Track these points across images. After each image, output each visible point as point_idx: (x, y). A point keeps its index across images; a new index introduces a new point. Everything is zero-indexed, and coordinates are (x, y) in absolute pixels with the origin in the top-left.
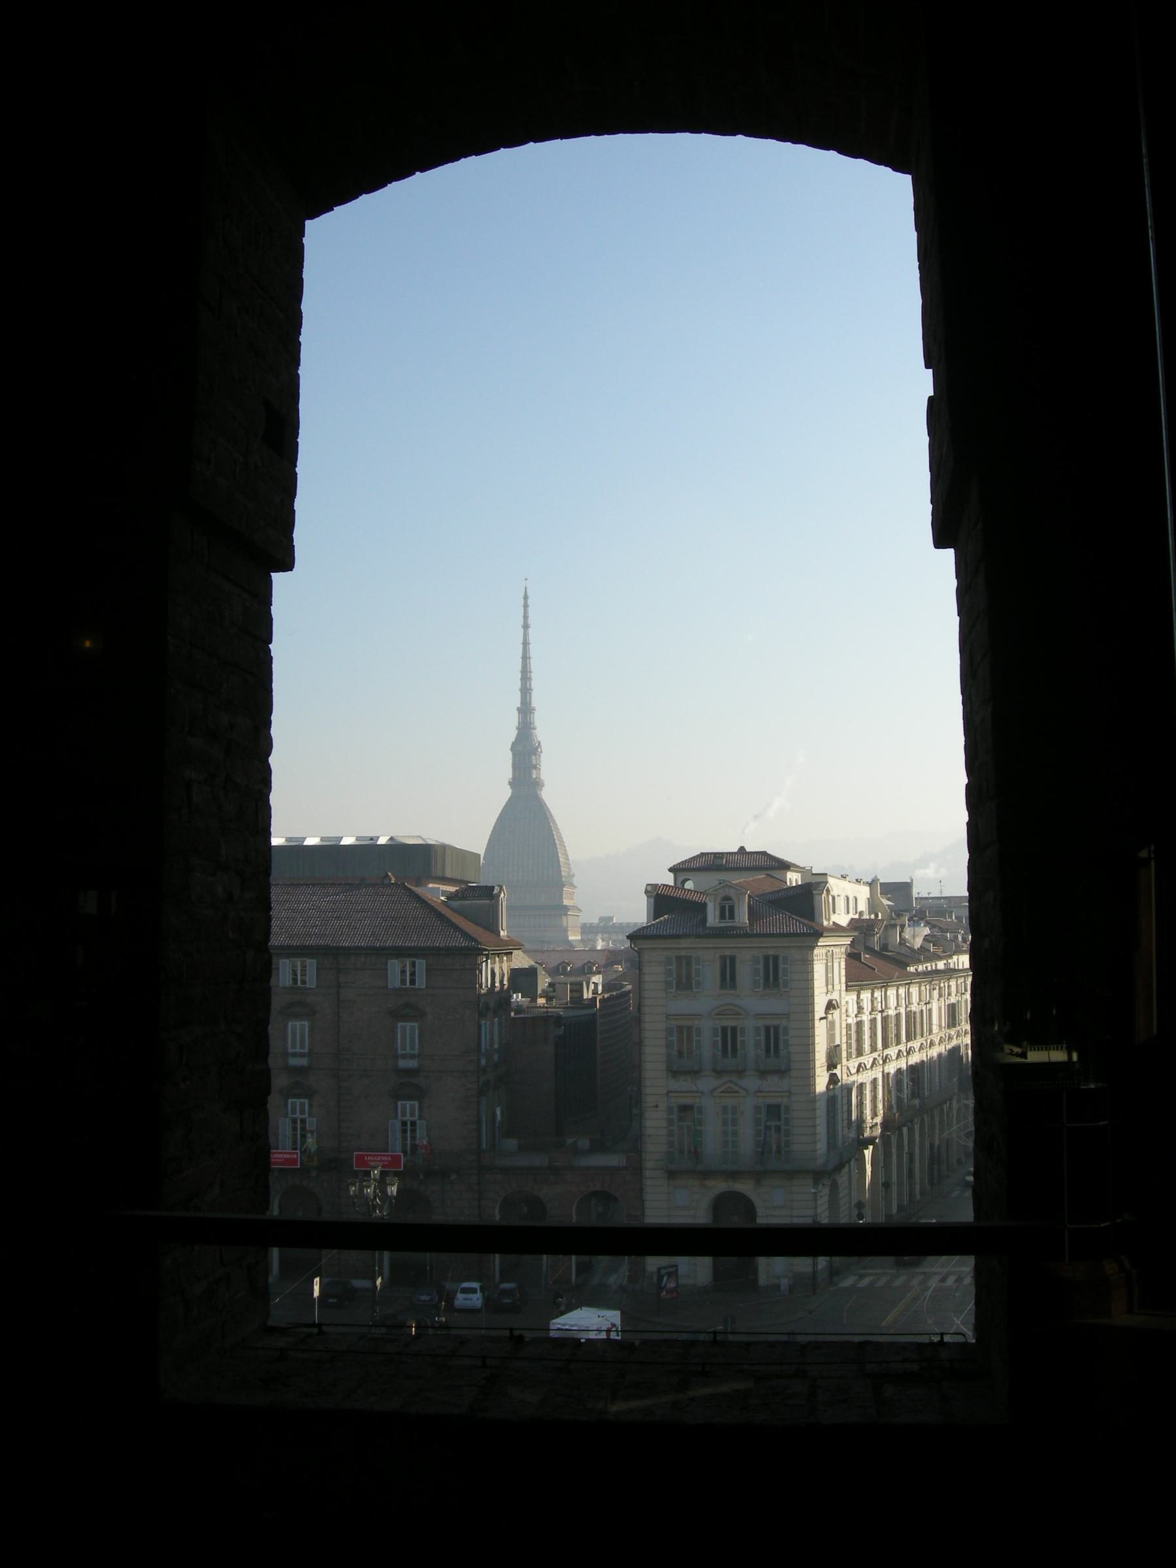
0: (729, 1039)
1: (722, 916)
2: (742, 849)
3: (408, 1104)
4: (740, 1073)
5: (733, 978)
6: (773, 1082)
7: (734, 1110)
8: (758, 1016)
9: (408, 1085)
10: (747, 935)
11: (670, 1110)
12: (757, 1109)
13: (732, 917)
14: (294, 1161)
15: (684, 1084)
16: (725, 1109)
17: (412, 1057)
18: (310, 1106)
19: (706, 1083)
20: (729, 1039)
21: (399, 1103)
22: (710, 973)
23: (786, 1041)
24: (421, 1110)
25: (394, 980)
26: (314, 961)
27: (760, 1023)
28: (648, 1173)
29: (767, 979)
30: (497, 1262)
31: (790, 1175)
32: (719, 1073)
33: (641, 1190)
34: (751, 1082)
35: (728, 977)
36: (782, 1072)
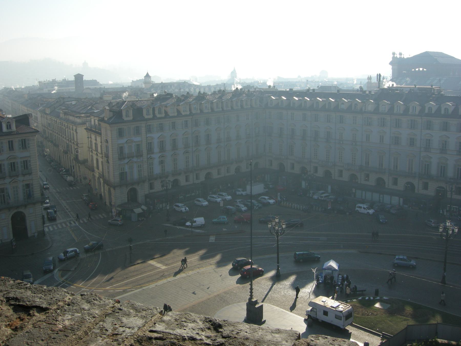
0: (13, 166)
1: (7, 128)
4: (17, 176)
5: (25, 146)
8: (21, 158)
10: (17, 134)
13: (10, 128)
19: (8, 180)
20: (13, 166)
22: (143, 130)
31: (34, 204)
32: (11, 177)
34: (21, 178)
35: (11, 147)
36: (30, 174)
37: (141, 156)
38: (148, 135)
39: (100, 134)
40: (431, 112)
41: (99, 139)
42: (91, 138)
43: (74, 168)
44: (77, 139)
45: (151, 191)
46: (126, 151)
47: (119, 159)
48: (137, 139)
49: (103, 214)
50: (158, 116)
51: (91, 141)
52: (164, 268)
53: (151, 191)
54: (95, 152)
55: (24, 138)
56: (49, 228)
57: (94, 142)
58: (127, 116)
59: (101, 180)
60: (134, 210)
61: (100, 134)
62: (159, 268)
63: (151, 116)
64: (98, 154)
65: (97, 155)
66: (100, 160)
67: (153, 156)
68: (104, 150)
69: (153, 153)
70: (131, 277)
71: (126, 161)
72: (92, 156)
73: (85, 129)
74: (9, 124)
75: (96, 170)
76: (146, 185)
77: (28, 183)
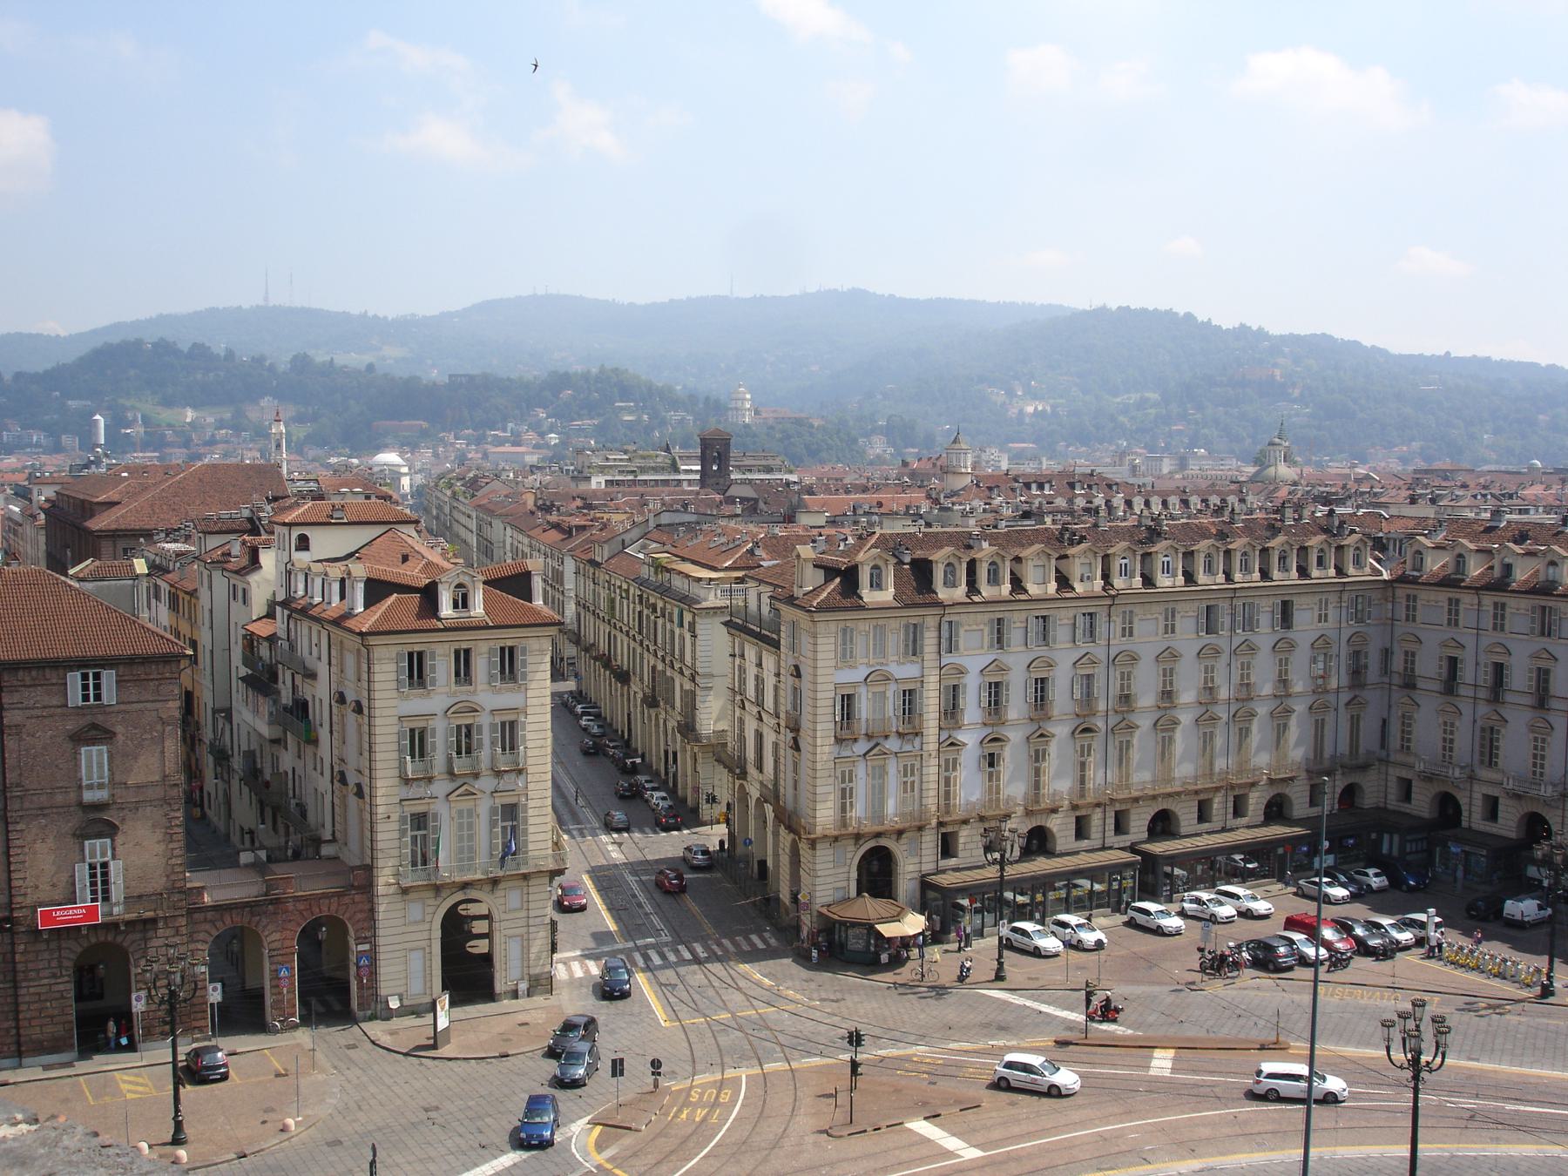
1: (456, 606)
2: (1448, 353)
3: (98, 842)
11: (402, 820)
12: (493, 811)
13: (465, 605)
17: (101, 786)
21: (87, 843)
22: (442, 667)
25: (75, 697)
27: (408, 725)
33: (372, 911)
38: (947, 659)
39: (776, 645)
41: (769, 662)
42: (742, 656)
44: (694, 658)
46: (864, 709)
48: (909, 671)
49: (767, 935)
51: (742, 670)
52: (973, 1153)
54: (755, 710)
55: (417, 648)
57: (752, 671)
59: (769, 808)
61: (776, 645)
62: (950, 1154)
66: (769, 738)
68: (786, 705)
71: (861, 747)
72: (741, 721)
73: (726, 624)
75: (752, 770)
76: (930, 841)
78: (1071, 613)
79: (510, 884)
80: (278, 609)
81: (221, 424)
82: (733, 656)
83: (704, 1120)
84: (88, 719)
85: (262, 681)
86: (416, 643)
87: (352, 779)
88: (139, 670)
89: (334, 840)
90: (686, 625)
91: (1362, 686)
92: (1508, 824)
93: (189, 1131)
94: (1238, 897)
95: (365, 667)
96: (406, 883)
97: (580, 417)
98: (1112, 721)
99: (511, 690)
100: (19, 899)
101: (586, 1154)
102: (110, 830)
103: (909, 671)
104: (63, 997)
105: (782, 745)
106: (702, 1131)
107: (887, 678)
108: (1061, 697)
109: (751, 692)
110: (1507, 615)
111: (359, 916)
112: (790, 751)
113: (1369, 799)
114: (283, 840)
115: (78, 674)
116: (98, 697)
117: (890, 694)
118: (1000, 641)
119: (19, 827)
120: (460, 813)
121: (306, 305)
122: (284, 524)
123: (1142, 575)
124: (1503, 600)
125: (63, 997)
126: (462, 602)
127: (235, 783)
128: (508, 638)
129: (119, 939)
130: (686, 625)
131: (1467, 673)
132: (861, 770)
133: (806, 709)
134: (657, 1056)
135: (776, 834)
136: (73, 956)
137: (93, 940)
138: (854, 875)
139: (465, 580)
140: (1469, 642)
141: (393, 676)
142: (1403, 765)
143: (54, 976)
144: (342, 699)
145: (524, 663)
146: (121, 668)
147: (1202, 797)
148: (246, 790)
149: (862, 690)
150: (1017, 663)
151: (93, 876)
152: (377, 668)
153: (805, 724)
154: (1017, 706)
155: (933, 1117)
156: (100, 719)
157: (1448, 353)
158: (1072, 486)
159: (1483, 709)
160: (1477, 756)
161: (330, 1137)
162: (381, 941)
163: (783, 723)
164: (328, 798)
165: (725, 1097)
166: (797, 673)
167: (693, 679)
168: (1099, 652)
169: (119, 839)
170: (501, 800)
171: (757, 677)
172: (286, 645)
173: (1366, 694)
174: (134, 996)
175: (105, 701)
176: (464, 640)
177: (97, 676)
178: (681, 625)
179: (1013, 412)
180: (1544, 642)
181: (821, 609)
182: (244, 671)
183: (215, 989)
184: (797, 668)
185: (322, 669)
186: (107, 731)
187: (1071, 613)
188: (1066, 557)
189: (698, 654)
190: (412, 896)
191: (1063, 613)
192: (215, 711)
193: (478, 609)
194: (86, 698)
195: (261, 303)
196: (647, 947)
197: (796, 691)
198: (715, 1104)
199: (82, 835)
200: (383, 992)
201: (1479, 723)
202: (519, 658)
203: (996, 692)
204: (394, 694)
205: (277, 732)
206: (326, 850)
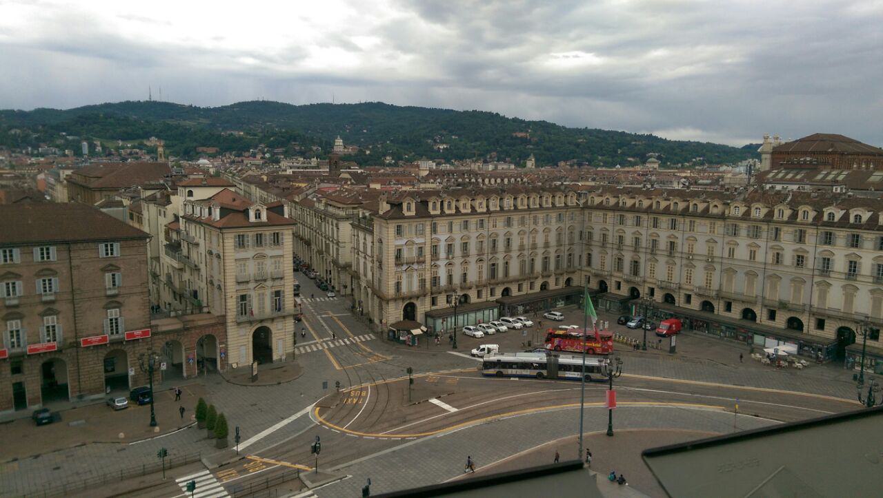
2: (586, 128)
3: (113, 310)
5: (278, 242)
6: (277, 283)
7: (263, 294)
9: (113, 301)
11: (237, 298)
12: (272, 293)
13: (260, 218)
14: (54, 347)
15: (242, 287)
16: (259, 294)
18: (58, 319)
21: (45, 318)
23: (795, 236)
24: (120, 312)
26: (55, 247)
27: (397, 248)
28: (229, 324)
29: (274, 242)
30: (619, 430)
33: (226, 332)
37: (424, 262)
38: (434, 236)
39: (372, 232)
40: (833, 219)
41: (369, 238)
42: (358, 236)
43: (330, 274)
44: (338, 236)
45: (434, 308)
46: (405, 254)
47: (395, 264)
48: (420, 240)
49: (370, 335)
50: (447, 212)
51: (358, 240)
52: (454, 410)
53: (434, 308)
54: (363, 255)
55: (277, 231)
56: (602, 479)
57: (362, 241)
58: (409, 209)
59: (369, 290)
60: (412, 331)
61: (372, 232)
62: (445, 411)
63: (438, 212)
64: (367, 257)
65: (365, 258)
66: (369, 265)
67: (438, 263)
68: (376, 252)
69: (438, 259)
70: (411, 421)
71: (405, 267)
72: (358, 258)
73: (351, 224)
74: (258, 212)
75: (362, 277)
76: (428, 300)
77: (279, 289)
78: (476, 220)
79: (278, 320)
80: (181, 219)
81: (134, 147)
82: (354, 236)
83: (357, 402)
84: (108, 263)
85: (174, 247)
86: (241, 231)
87: (216, 284)
88: (130, 243)
89: (208, 306)
90: (334, 225)
91: (573, 244)
92: (625, 291)
93: (158, 420)
94: (510, 322)
95: (221, 240)
96: (238, 321)
97: (278, 147)
98: (490, 257)
99: (277, 249)
100: (80, 334)
101: (315, 418)
102: (119, 305)
103: (420, 240)
104: (99, 372)
105: (375, 267)
106: (355, 408)
107: (413, 243)
108: (473, 249)
109: (361, 249)
110: (696, 225)
111: (221, 334)
112: (378, 269)
113: (575, 283)
114: (184, 306)
115: (103, 245)
116: (48, 258)
117: (414, 249)
118: (451, 230)
119: (79, 305)
120: (259, 294)
121: (167, 101)
122: (183, 186)
123: (500, 206)
124: (639, 215)
125: (99, 372)
126: (258, 216)
127: (162, 286)
128: (276, 229)
129: (123, 348)
130: (334, 225)
131: (610, 239)
132: (404, 276)
133: (385, 254)
134: (408, 367)
135: (373, 299)
136: (104, 355)
137: (112, 349)
138: (402, 313)
139: (260, 208)
140: (610, 228)
141: (233, 244)
142: (587, 271)
143: (95, 364)
144: (211, 253)
145: (282, 239)
146: (122, 242)
147: (520, 282)
148: (167, 288)
149: (405, 247)
150: (458, 235)
151: (112, 323)
152: (226, 241)
153: (384, 261)
154: (458, 251)
155: (438, 398)
156: (113, 263)
157: (586, 128)
158: (464, 174)
159: (615, 252)
160: (613, 268)
161: (40, 458)
162: (229, 343)
163: (375, 259)
164: (205, 290)
165: (364, 394)
166: (380, 241)
167: (338, 245)
168: (486, 234)
169: (122, 308)
170: (274, 290)
171: (364, 243)
172: (185, 233)
173: (574, 247)
174: (130, 369)
175: (51, 259)
176: (259, 230)
177: (112, 245)
178: (332, 225)
179: (436, 148)
180: (673, 232)
181: (390, 219)
182: (165, 242)
183: (132, 370)
184: (381, 240)
185: (202, 242)
186: (116, 267)
187: (476, 220)
188: (474, 200)
189: (340, 235)
190: (241, 326)
191: (473, 220)
192: (151, 258)
193: (264, 218)
194: (107, 254)
195: (149, 100)
196: (328, 341)
197: (380, 248)
198: (360, 397)
199: (107, 308)
200: (230, 362)
201: (614, 257)
202: (280, 237)
203: (465, 246)
204: (233, 251)
205: (181, 266)
206: (205, 310)
